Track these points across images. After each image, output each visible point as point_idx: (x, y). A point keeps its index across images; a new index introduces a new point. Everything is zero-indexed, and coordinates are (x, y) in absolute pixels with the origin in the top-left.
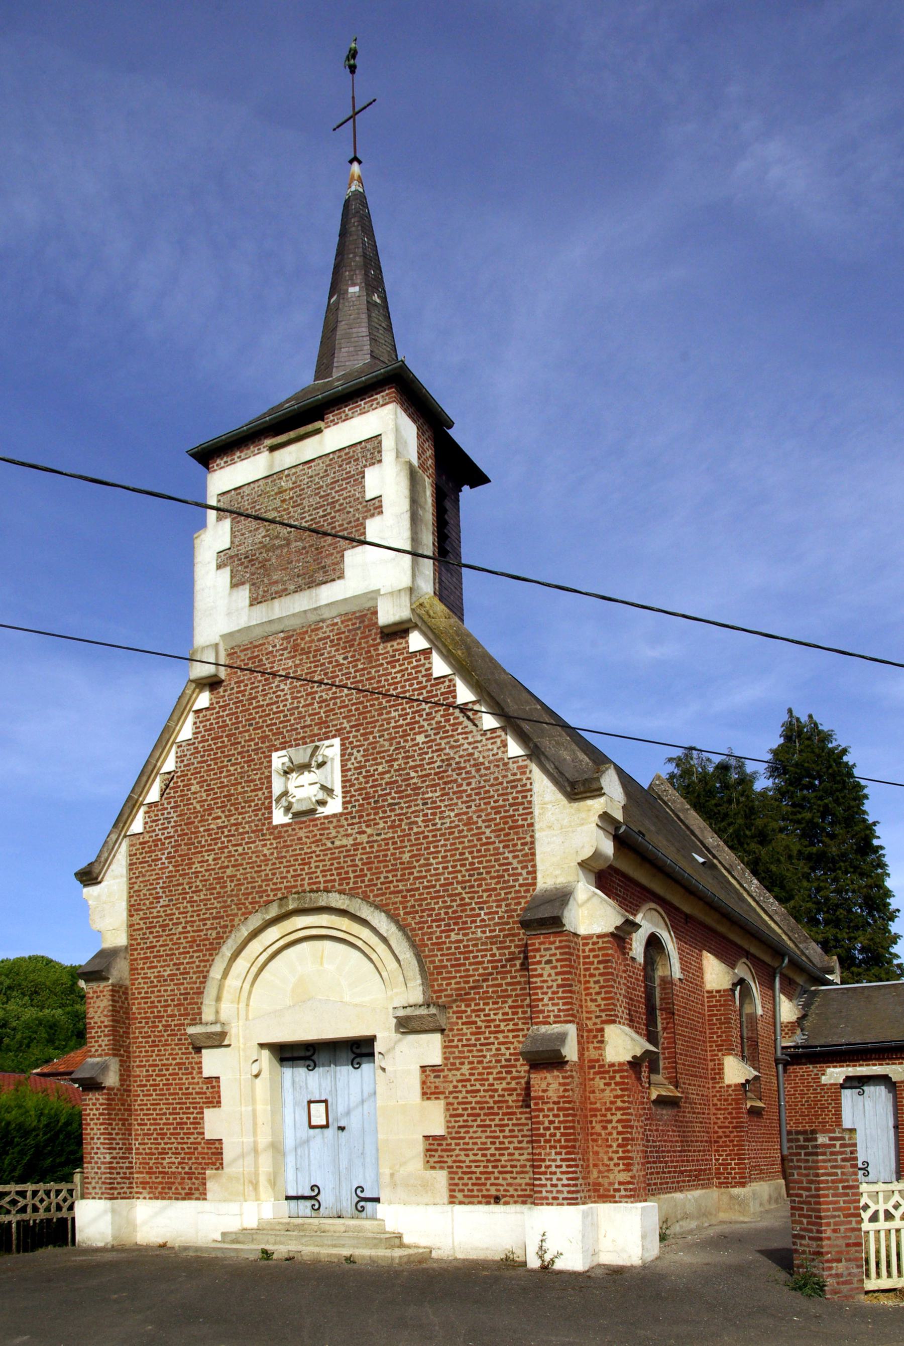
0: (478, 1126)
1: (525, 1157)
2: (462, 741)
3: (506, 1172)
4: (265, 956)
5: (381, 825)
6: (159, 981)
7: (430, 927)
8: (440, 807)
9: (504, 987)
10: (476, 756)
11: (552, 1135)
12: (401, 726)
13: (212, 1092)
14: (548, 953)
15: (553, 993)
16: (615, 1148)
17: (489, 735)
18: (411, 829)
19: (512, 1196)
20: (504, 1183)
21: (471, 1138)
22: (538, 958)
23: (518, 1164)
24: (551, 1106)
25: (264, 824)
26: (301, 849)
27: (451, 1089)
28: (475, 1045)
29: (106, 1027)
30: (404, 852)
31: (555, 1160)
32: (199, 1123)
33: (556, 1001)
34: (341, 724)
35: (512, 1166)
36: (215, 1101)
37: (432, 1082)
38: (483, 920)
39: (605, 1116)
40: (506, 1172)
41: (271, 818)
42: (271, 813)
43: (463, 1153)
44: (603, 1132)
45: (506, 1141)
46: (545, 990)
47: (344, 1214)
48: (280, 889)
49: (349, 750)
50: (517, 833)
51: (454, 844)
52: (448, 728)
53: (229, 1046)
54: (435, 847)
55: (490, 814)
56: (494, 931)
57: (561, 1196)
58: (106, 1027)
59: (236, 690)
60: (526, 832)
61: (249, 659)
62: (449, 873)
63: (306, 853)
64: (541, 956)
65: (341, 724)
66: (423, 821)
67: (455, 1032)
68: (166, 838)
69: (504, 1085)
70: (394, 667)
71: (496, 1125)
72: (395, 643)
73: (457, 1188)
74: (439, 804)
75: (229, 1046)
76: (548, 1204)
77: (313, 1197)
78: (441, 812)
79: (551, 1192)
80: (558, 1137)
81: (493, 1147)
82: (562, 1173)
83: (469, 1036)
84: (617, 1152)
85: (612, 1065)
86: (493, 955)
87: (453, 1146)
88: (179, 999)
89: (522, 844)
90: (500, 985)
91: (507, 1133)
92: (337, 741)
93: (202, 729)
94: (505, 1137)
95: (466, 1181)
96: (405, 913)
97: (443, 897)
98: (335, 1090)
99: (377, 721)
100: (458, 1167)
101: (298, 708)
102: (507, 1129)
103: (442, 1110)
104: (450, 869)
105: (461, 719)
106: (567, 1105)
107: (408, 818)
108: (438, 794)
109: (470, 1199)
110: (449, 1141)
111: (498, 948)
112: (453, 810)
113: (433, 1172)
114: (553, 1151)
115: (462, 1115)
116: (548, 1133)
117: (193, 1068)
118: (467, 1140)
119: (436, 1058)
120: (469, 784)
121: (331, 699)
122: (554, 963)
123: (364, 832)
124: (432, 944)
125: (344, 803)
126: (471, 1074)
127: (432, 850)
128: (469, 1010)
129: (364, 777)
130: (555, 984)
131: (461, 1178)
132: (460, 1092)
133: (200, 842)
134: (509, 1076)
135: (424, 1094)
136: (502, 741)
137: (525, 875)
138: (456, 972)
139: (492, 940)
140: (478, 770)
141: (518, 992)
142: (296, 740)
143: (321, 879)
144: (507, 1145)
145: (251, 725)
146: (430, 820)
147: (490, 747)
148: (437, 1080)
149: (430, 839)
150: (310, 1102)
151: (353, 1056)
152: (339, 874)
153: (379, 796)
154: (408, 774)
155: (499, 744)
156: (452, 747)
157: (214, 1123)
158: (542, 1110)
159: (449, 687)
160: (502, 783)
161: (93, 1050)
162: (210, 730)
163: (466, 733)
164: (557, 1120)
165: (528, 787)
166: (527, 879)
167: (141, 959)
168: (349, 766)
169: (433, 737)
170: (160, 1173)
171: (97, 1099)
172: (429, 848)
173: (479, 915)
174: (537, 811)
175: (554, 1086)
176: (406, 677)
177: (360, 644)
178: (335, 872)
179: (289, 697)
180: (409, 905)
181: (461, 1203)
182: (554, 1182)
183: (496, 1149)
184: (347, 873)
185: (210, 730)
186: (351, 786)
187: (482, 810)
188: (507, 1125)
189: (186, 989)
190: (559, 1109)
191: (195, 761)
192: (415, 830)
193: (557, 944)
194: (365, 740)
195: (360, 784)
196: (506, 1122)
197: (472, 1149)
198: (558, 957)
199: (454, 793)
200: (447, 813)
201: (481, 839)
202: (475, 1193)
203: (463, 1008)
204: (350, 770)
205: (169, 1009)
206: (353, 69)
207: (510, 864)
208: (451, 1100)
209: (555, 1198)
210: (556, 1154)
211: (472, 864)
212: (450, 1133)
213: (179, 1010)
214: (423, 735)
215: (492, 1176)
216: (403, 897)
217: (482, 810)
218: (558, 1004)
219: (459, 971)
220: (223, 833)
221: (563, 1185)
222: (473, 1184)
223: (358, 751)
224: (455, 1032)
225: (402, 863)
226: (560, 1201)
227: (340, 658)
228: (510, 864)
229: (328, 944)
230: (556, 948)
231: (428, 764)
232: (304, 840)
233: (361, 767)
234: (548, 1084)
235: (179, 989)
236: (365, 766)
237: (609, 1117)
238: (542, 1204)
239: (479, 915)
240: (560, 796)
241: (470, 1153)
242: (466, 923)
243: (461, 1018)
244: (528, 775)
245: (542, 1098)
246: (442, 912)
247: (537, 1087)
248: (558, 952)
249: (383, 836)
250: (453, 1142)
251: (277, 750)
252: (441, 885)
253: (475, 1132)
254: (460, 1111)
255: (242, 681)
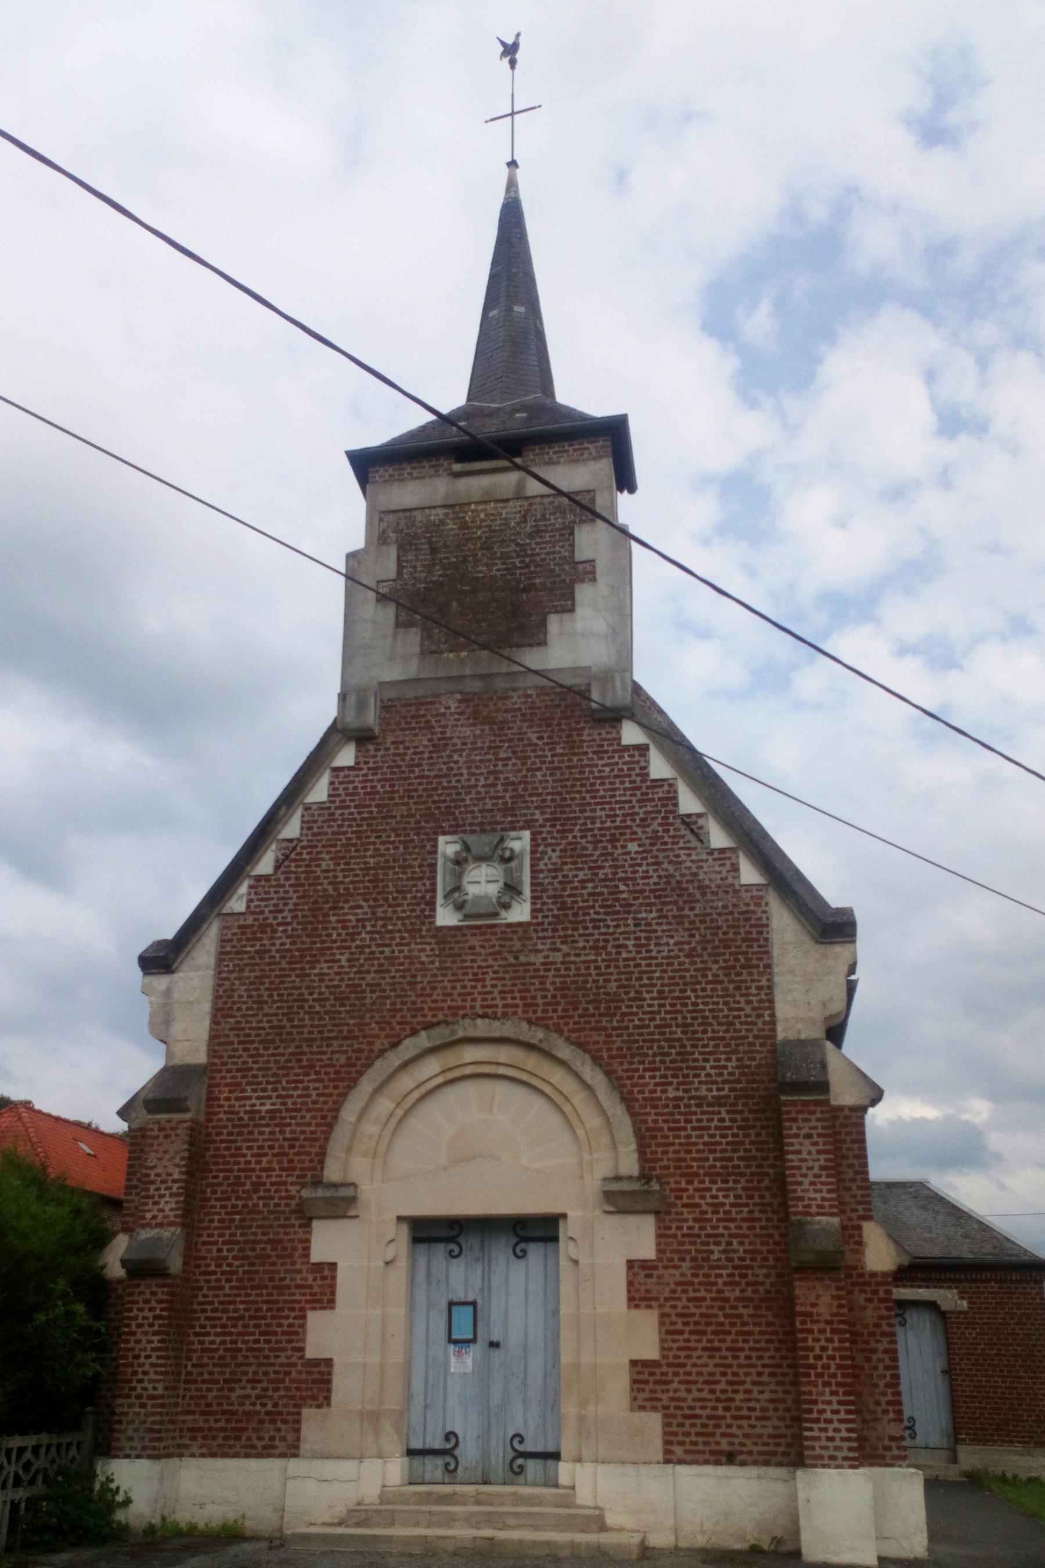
0: (704, 1349)
1: (766, 1396)
2: (684, 857)
3: (742, 1418)
4: (416, 1094)
5: (581, 944)
6: (251, 1119)
7: (642, 1077)
8: (656, 931)
9: (736, 1162)
10: (701, 877)
11: (824, 1367)
12: (609, 829)
13: (322, 1287)
14: (807, 1124)
15: (815, 1176)
16: (881, 1388)
17: (716, 855)
18: (620, 953)
19: (750, 1453)
20: (739, 1433)
21: (694, 1365)
22: (795, 1131)
23: (758, 1406)
24: (822, 1326)
25: (423, 924)
26: (473, 961)
27: (667, 1294)
28: (699, 1236)
29: (175, 1181)
30: (609, 981)
31: (830, 1403)
32: (296, 1333)
33: (819, 1187)
34: (532, 814)
35: (750, 1409)
36: (326, 1300)
37: (642, 1283)
38: (708, 1075)
39: (867, 1342)
40: (742, 1418)
41: (434, 917)
42: (434, 910)
43: (683, 1387)
44: (866, 1366)
45: (741, 1371)
46: (804, 1171)
47: (492, 1478)
48: (441, 1009)
49: (541, 848)
50: (751, 974)
51: (673, 978)
52: (666, 839)
53: (356, 1217)
54: (649, 979)
55: (717, 947)
56: (723, 1089)
57: (840, 1454)
58: (175, 1181)
59: (392, 751)
60: (761, 974)
61: (413, 717)
62: (667, 1012)
63: (479, 967)
64: (799, 1128)
65: (532, 814)
66: (634, 945)
67: (673, 1216)
68: (279, 924)
69: (737, 1293)
70: (602, 758)
71: (727, 1349)
72: (603, 732)
73: (674, 1439)
74: (654, 927)
75: (356, 1217)
76: (823, 1466)
77: (447, 1451)
78: (658, 938)
79: (826, 1448)
80: (833, 1370)
81: (724, 1379)
82: (841, 1421)
83: (691, 1223)
84: (884, 1394)
85: (874, 1275)
86: (722, 1120)
87: (670, 1377)
88: (281, 1147)
89: (757, 988)
90: (731, 1159)
91: (742, 1361)
92: (527, 834)
93: (341, 791)
94: (740, 1366)
95: (687, 1429)
96: (610, 1057)
97: (659, 1041)
98: (486, 1288)
99: (579, 818)
100: (677, 1408)
101: (476, 786)
102: (742, 1355)
103: (656, 1323)
104: (668, 1008)
105: (683, 832)
106: (842, 1326)
107: (615, 940)
108: (654, 915)
109: (692, 1458)
110: (664, 1369)
111: (728, 1112)
112: (672, 937)
113: (643, 1414)
114: (827, 1390)
115: (681, 1332)
116: (820, 1363)
117: (295, 1249)
118: (688, 1368)
119: (647, 1251)
120: (692, 909)
121: (520, 783)
122: (815, 1139)
123: (558, 950)
124: (644, 1099)
125: (533, 911)
126: (695, 1275)
127: (645, 981)
128: (690, 1187)
129: (560, 883)
130: (816, 1164)
131: (681, 1425)
132: (679, 1299)
133: (329, 935)
134: (743, 1281)
135: (630, 1299)
136: (732, 864)
137: (760, 1025)
138: (675, 1137)
139: (719, 1101)
140: (704, 894)
141: (754, 1169)
142: (470, 825)
143: (500, 1003)
144: (742, 1378)
145: (411, 797)
146: (644, 946)
147: (717, 868)
148: (648, 1280)
149: (644, 968)
150: (451, 1304)
151: (515, 1240)
152: (523, 998)
153: (579, 908)
154: (617, 886)
155: (728, 867)
156: (671, 862)
157: (323, 1334)
158: (811, 1331)
159: (669, 792)
160: (732, 913)
161: (148, 1215)
162: (353, 794)
163: (689, 848)
164: (830, 1346)
165: (764, 921)
166: (762, 1030)
167: (226, 1085)
168: (542, 866)
169: (648, 848)
170: (224, 1412)
171: (154, 1294)
172: (641, 979)
173: (704, 1068)
174: (776, 952)
175: (826, 1299)
176: (616, 772)
177: (559, 724)
178: (518, 995)
179: (465, 771)
180: (615, 1046)
181: (681, 1462)
182: (831, 1434)
183: (729, 1383)
184: (534, 998)
185: (353, 794)
186: (542, 891)
187: (708, 942)
188: (742, 1349)
189: (293, 1132)
190: (833, 1331)
191: (329, 830)
192: (624, 955)
193: (818, 1115)
194: (562, 838)
195: (555, 890)
196: (740, 1345)
197: (696, 1382)
198: (820, 1131)
199: (674, 917)
200: (664, 940)
201: (706, 976)
202: (701, 1447)
203: (683, 1185)
204: (542, 871)
205: (264, 1160)
206: (513, 164)
207: (742, 1009)
208: (667, 1310)
209: (832, 1458)
210: (832, 1393)
211: (695, 1004)
212: (664, 1357)
213: (279, 1162)
214: (635, 844)
215: (723, 1422)
216: (607, 1036)
217: (708, 942)
218: (820, 1191)
219: (679, 1137)
220: (364, 927)
221: (843, 1439)
222: (698, 1434)
223: (554, 851)
224: (673, 1216)
225: (608, 994)
226: (839, 1462)
227: (534, 737)
228: (742, 1009)
229: (501, 1087)
230: (818, 1120)
231: (642, 878)
232: (478, 950)
233: (556, 870)
234: (818, 1297)
235: (282, 1132)
236: (562, 870)
237: (873, 1345)
238: (815, 1466)
239: (704, 1068)
240: (805, 938)
241: (694, 1387)
242: (687, 1076)
243: (681, 1198)
244: (763, 908)
245: (810, 1314)
246: (658, 1059)
247: (802, 1300)
248: (819, 1124)
249: (582, 958)
250: (670, 1370)
251: (445, 833)
252: (656, 1027)
253: (699, 1357)
254: (679, 1327)
255: (402, 742)
